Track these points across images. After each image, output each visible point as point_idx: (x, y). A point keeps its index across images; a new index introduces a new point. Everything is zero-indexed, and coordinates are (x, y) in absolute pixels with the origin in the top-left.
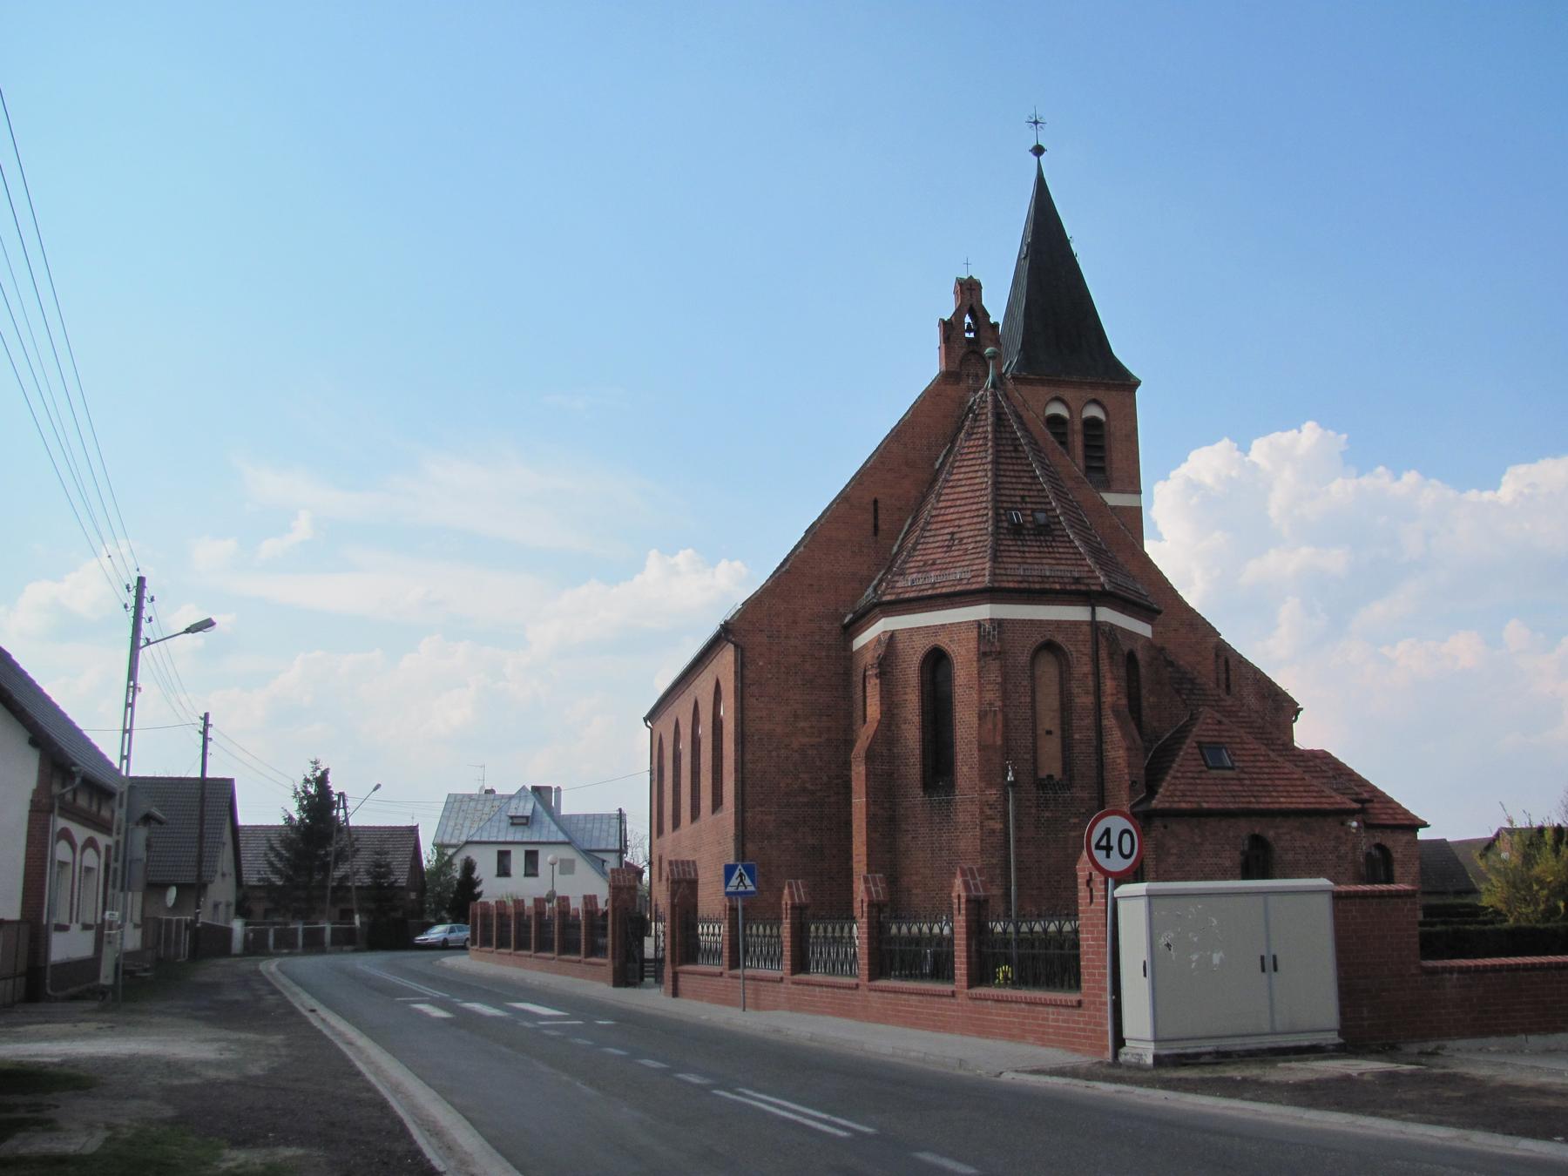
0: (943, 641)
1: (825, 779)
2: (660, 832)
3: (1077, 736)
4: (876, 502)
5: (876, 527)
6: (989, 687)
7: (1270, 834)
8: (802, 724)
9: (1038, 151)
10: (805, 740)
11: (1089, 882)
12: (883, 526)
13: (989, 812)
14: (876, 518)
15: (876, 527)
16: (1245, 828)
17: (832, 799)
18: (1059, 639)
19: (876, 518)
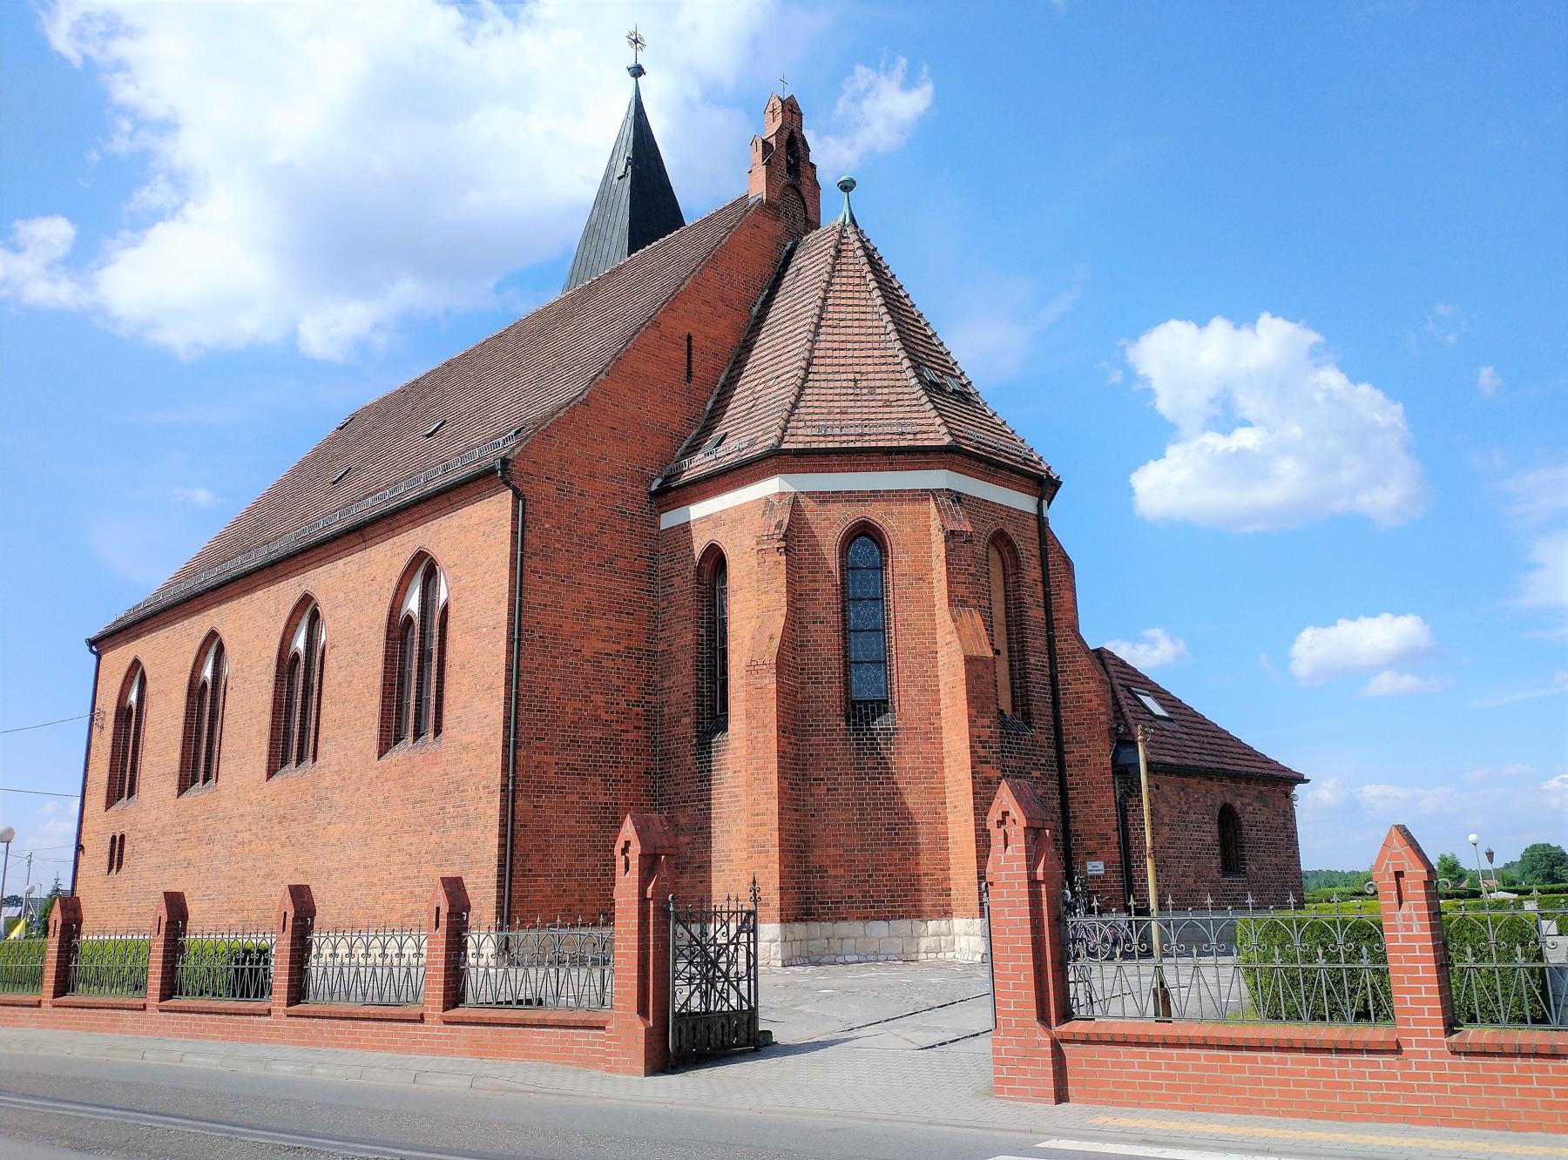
0: (874, 513)
1: (623, 705)
2: (122, 784)
3: (1032, 661)
4: (689, 338)
5: (689, 373)
6: (961, 578)
7: (1237, 804)
8: (597, 622)
9: (637, 71)
10: (599, 645)
11: (625, 851)
12: (696, 372)
13: (982, 752)
14: (689, 362)
15: (689, 373)
16: (1219, 793)
17: (630, 736)
18: (1010, 530)
19: (689, 362)
